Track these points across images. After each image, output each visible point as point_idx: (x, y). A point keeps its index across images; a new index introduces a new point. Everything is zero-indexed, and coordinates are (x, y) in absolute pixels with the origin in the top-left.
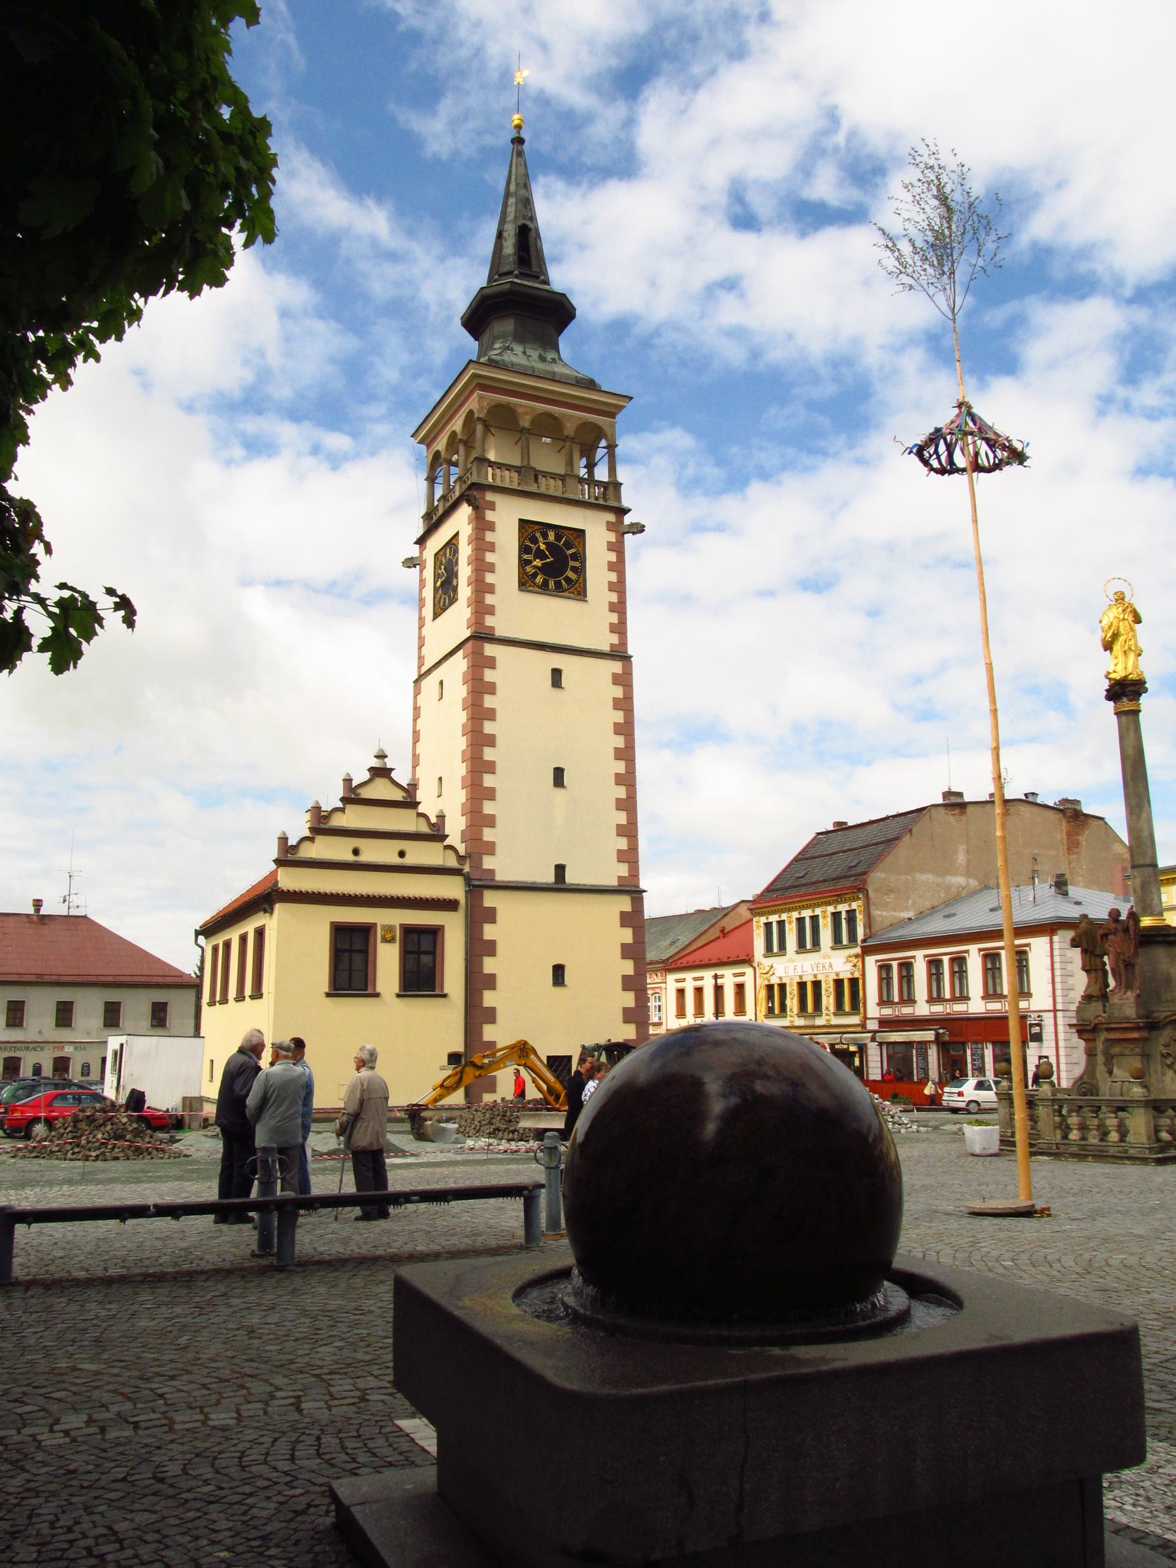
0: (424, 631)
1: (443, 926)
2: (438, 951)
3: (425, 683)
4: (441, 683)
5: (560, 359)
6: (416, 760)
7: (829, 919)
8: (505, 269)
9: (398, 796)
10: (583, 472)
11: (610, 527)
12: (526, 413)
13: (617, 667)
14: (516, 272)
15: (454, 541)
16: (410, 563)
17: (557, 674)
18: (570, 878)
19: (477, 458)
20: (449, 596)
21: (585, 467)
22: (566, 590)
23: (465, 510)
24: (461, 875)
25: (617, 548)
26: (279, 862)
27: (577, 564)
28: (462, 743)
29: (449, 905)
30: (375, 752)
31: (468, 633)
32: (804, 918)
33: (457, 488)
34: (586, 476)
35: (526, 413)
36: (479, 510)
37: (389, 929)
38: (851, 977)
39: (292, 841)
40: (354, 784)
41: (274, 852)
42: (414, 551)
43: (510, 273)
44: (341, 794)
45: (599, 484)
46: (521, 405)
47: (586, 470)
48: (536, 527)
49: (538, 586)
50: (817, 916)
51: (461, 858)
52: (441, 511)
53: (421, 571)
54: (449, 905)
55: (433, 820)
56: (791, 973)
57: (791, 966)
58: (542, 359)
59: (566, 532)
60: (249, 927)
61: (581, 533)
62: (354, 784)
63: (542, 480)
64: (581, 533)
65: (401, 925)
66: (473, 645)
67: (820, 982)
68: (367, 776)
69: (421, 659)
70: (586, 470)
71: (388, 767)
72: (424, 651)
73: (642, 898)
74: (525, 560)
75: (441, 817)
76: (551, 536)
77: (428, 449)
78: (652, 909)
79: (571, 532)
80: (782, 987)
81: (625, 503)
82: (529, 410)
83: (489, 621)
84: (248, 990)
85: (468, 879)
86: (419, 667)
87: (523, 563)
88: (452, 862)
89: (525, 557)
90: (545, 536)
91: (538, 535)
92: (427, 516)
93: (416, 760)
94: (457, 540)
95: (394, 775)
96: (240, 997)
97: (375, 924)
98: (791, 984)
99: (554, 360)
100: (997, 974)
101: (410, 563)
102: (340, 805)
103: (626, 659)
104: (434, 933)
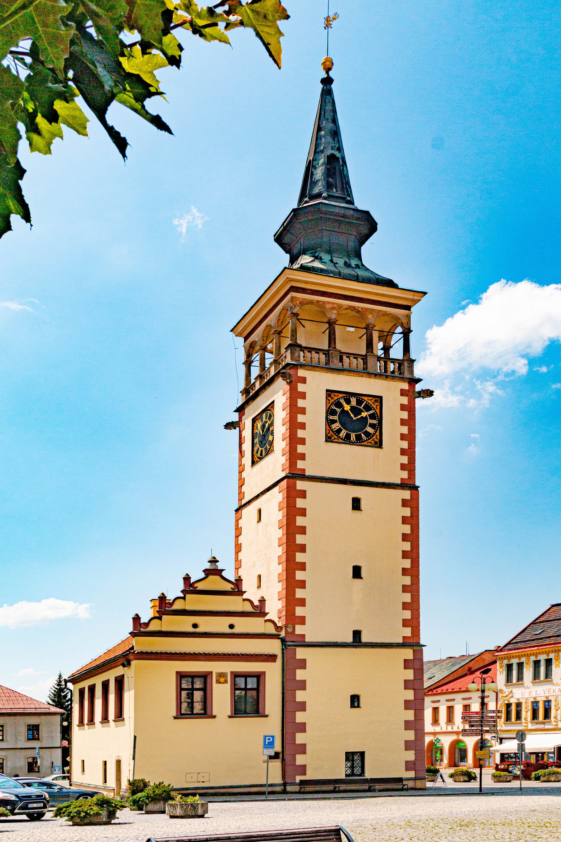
0: (244, 475)
1: (264, 672)
2: (261, 688)
3: (245, 511)
4: (260, 511)
5: (363, 265)
6: (238, 564)
7: (532, 664)
8: (316, 191)
9: (229, 587)
10: (380, 353)
11: (403, 393)
12: (333, 308)
13: (406, 494)
14: (325, 195)
15: (270, 408)
16: (230, 426)
17: (356, 504)
18: (365, 639)
19: (290, 346)
20: (266, 449)
21: (382, 349)
22: (365, 441)
23: (281, 384)
24: (279, 638)
25: (410, 409)
26: (133, 634)
27: (375, 422)
28: (280, 551)
29: (271, 658)
30: (209, 558)
31: (283, 475)
32: (512, 665)
33: (273, 368)
34: (383, 356)
35: (333, 308)
36: (292, 383)
37: (221, 675)
38: (517, 702)
39: (144, 620)
40: (192, 581)
41: (130, 628)
42: (235, 417)
43: (319, 196)
44: (182, 588)
45: (394, 361)
46: (329, 303)
47: (383, 351)
48: (341, 395)
49: (342, 439)
50: (551, 659)
51: (277, 628)
52: (258, 386)
53: (240, 432)
54: (271, 658)
55: (256, 603)
56: (527, 695)
57: (527, 691)
58: (347, 265)
59: (366, 398)
60: (111, 675)
61: (379, 399)
62: (192, 581)
63: (346, 360)
64: (379, 399)
65: (232, 672)
66: (287, 483)
67: (550, 701)
68: (203, 575)
69: (241, 494)
70: (383, 351)
71: (219, 568)
72: (244, 489)
73: (422, 651)
74: (331, 420)
75: (262, 601)
76: (354, 401)
77: (245, 341)
78: (428, 655)
79: (370, 398)
80: (519, 705)
81: (417, 374)
82: (335, 306)
83: (300, 464)
84: (86, 721)
85: (283, 641)
86: (240, 500)
87: (330, 422)
88: (271, 630)
89: (331, 417)
90: (348, 402)
91: (342, 401)
92: (246, 391)
93: (238, 564)
94: (273, 407)
95: (224, 574)
96: (105, 718)
97: (211, 672)
98: (526, 702)
99: (357, 266)
100: (451, 711)
101: (230, 426)
102: (182, 595)
103: (414, 488)
104: (259, 677)
